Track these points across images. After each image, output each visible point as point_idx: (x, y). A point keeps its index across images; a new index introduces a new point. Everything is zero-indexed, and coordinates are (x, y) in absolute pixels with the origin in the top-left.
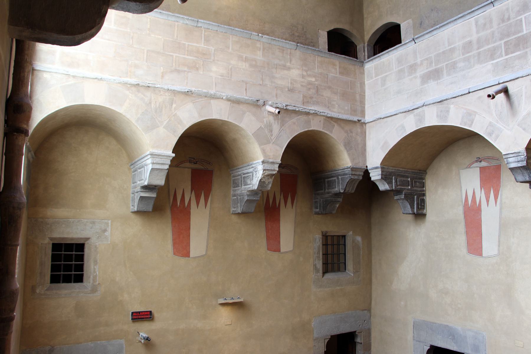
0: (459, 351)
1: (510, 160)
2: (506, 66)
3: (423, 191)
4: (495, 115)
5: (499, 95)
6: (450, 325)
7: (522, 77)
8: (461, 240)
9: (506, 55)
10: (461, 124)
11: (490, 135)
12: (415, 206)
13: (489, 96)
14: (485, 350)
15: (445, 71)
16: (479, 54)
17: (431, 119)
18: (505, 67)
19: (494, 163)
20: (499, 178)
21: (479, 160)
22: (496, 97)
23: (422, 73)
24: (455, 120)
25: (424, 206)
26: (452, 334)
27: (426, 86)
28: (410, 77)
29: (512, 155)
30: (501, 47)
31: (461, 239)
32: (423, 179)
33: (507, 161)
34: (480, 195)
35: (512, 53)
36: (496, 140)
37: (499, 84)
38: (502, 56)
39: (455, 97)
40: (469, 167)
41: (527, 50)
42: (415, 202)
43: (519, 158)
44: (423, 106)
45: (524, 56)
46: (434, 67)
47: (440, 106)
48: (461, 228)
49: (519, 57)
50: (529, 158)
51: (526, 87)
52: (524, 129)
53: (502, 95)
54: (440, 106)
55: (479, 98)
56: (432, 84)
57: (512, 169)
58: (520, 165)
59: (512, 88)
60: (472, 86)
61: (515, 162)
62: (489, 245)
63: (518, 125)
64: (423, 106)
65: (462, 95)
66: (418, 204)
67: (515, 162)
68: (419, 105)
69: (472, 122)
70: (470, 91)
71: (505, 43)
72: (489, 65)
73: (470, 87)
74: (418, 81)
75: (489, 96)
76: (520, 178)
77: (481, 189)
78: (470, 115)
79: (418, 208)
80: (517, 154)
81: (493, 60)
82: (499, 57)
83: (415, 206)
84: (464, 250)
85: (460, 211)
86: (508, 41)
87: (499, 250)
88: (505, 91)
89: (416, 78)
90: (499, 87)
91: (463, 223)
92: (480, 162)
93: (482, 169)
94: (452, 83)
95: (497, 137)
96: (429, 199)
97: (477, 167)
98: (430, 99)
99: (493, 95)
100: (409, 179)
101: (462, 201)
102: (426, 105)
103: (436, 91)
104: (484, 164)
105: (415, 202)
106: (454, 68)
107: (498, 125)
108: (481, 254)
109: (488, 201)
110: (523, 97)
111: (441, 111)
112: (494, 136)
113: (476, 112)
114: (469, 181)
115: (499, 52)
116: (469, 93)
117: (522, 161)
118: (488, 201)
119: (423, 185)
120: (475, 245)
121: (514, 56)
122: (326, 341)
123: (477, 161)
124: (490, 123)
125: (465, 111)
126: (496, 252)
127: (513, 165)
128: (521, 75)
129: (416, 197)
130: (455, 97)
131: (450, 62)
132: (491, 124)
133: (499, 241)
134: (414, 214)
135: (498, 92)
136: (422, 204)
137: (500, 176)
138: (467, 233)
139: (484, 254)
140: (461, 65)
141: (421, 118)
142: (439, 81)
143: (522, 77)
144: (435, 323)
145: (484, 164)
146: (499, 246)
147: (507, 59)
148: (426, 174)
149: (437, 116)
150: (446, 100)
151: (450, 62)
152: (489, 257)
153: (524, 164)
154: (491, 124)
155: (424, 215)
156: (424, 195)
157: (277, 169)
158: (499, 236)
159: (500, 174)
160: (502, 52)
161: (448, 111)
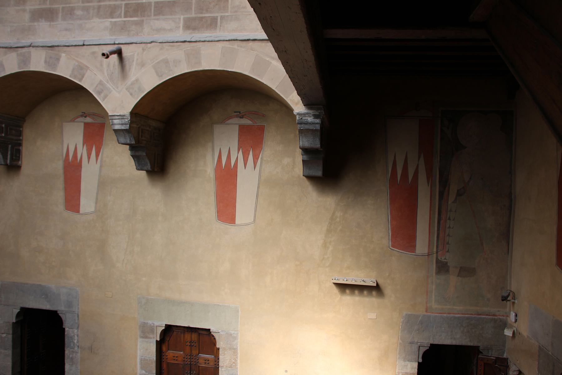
0: (51, 309)
1: (115, 121)
2: (123, 28)
3: (20, 140)
4: (106, 74)
5: (113, 56)
6: (43, 284)
7: (136, 43)
8: (59, 195)
9: (125, 17)
10: (70, 76)
11: (99, 93)
12: (9, 157)
13: (103, 55)
14: (78, 305)
15: (60, 15)
16: (99, 7)
17: (38, 63)
18: (122, 29)
19: (99, 120)
20: (102, 136)
21: (84, 115)
22: (110, 57)
23: (33, 7)
24: (64, 70)
25: (19, 157)
26: (45, 292)
27: (36, 24)
28: (17, 8)
29: (117, 117)
30: (122, 7)
31: (59, 195)
32: (22, 127)
33: (112, 122)
34: (82, 151)
35: (131, 17)
36: (104, 100)
37: (114, 44)
38: (121, 17)
39: (68, 46)
40: (73, 120)
41: (144, 19)
42: (9, 153)
43: (123, 121)
44: (30, 46)
45: (140, 24)
46: (47, 6)
47: (50, 51)
48: (60, 184)
49: (136, 23)
50: (132, 122)
51: (138, 54)
52: (131, 94)
53: (115, 57)
54: (50, 51)
55: (94, 53)
56: (43, 25)
57: (116, 131)
58: (123, 127)
59: (126, 51)
60: (88, 38)
61: (120, 124)
62: (87, 203)
63: (127, 89)
64: (30, 46)
65: (76, 46)
66: (12, 155)
67: (120, 124)
68: (25, 45)
69: (83, 77)
70: (85, 44)
71: (126, 5)
72: (108, 22)
73: (86, 39)
74: (27, 16)
75: (103, 55)
76: (122, 140)
77: (83, 145)
78: (81, 69)
79: (12, 159)
80: (122, 117)
81: (113, 18)
82: (118, 17)
83: (9, 157)
84: (61, 207)
85: (60, 165)
86: (128, 4)
87: (96, 207)
88: (119, 53)
89: (24, 11)
90: (114, 48)
91: (62, 179)
92: (85, 117)
93: (86, 125)
94: (66, 30)
95: (106, 97)
96: (25, 150)
97: (82, 122)
98: (39, 40)
99: (107, 55)
100: (3, 126)
101: (63, 156)
102: (33, 47)
103: (46, 33)
104: (88, 120)
105: (9, 153)
106: (71, 14)
107: (108, 85)
108: (78, 211)
109: (89, 158)
110: (135, 63)
111: (51, 57)
112: (102, 95)
113: (88, 68)
114: (73, 137)
115: (119, 12)
116: (84, 45)
117: (126, 124)
118: (89, 158)
119: (20, 134)
120: (72, 202)
121: (132, 21)
122: (423, 350)
123: (82, 116)
124: (101, 81)
125: (77, 64)
126: (93, 209)
127: (117, 127)
128: (135, 41)
129: (10, 146)
130: (68, 46)
131: (67, 5)
132: (101, 83)
133: (97, 199)
134: (7, 165)
135: (112, 53)
136: (17, 155)
137: (103, 135)
138: (66, 189)
139: (82, 210)
140: (79, 13)
141: (26, 60)
142: (52, 23)
143: (136, 43)
144: (27, 284)
145: (88, 120)
146: (96, 203)
147: (125, 21)
148: (25, 121)
149: (46, 62)
150: (58, 46)
151: (67, 5)
152: (86, 214)
153: (127, 127)
154: (101, 83)
155: (19, 168)
156: (20, 145)
157: (129, 118)
158: (97, 194)
159: (103, 132)
160: (121, 12)
161: (58, 59)
